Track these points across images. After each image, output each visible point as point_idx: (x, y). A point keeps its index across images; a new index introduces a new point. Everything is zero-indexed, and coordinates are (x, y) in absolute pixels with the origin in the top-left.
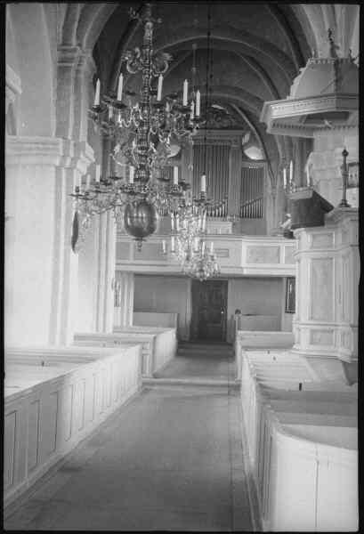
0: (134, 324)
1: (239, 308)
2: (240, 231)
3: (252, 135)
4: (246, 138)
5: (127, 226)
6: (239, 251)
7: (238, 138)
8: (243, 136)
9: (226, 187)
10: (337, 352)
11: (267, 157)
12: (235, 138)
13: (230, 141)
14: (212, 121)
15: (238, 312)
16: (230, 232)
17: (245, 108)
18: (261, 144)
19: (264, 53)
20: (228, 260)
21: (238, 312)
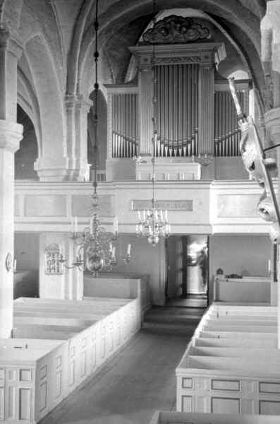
0: (86, 294)
1: (222, 268)
2: (213, 173)
3: (229, 49)
4: (221, 55)
5: (203, 252)
6: (205, 204)
7: (210, 53)
8: (215, 50)
9: (196, 108)
10: (59, 22)
11: (254, 76)
12: (205, 54)
13: (199, 58)
14: (176, 33)
15: (220, 272)
16: (198, 177)
17: (215, 13)
18: (247, 65)
19: (234, 14)
20: (110, 156)
21: (220, 272)
